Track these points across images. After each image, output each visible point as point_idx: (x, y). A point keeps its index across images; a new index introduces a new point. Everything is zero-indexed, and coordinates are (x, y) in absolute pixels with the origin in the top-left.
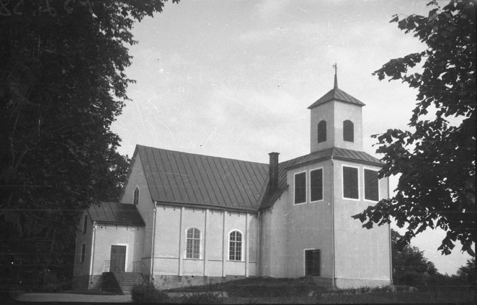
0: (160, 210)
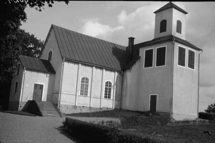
0: (66, 64)
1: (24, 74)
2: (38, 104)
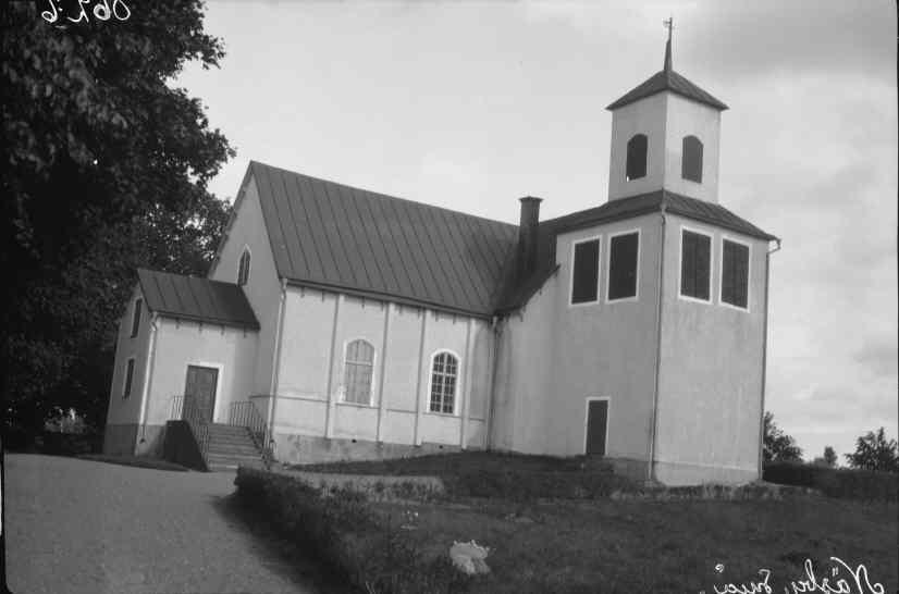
0: (293, 297)
1: (156, 333)
2: (197, 430)
